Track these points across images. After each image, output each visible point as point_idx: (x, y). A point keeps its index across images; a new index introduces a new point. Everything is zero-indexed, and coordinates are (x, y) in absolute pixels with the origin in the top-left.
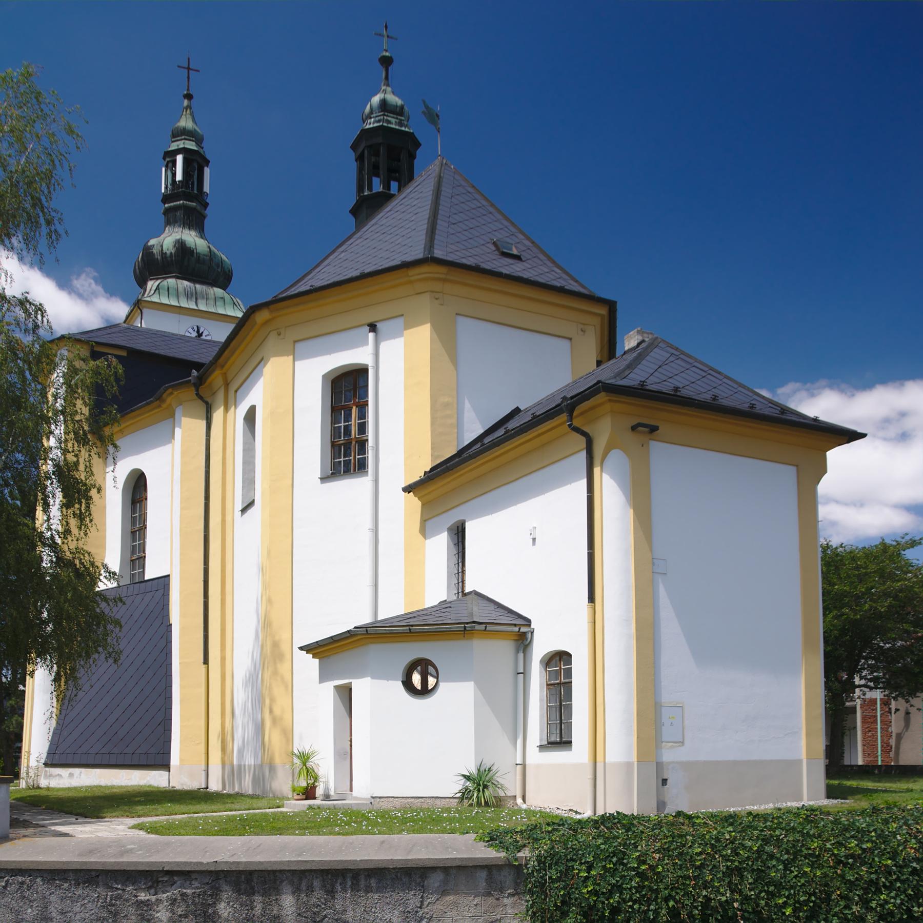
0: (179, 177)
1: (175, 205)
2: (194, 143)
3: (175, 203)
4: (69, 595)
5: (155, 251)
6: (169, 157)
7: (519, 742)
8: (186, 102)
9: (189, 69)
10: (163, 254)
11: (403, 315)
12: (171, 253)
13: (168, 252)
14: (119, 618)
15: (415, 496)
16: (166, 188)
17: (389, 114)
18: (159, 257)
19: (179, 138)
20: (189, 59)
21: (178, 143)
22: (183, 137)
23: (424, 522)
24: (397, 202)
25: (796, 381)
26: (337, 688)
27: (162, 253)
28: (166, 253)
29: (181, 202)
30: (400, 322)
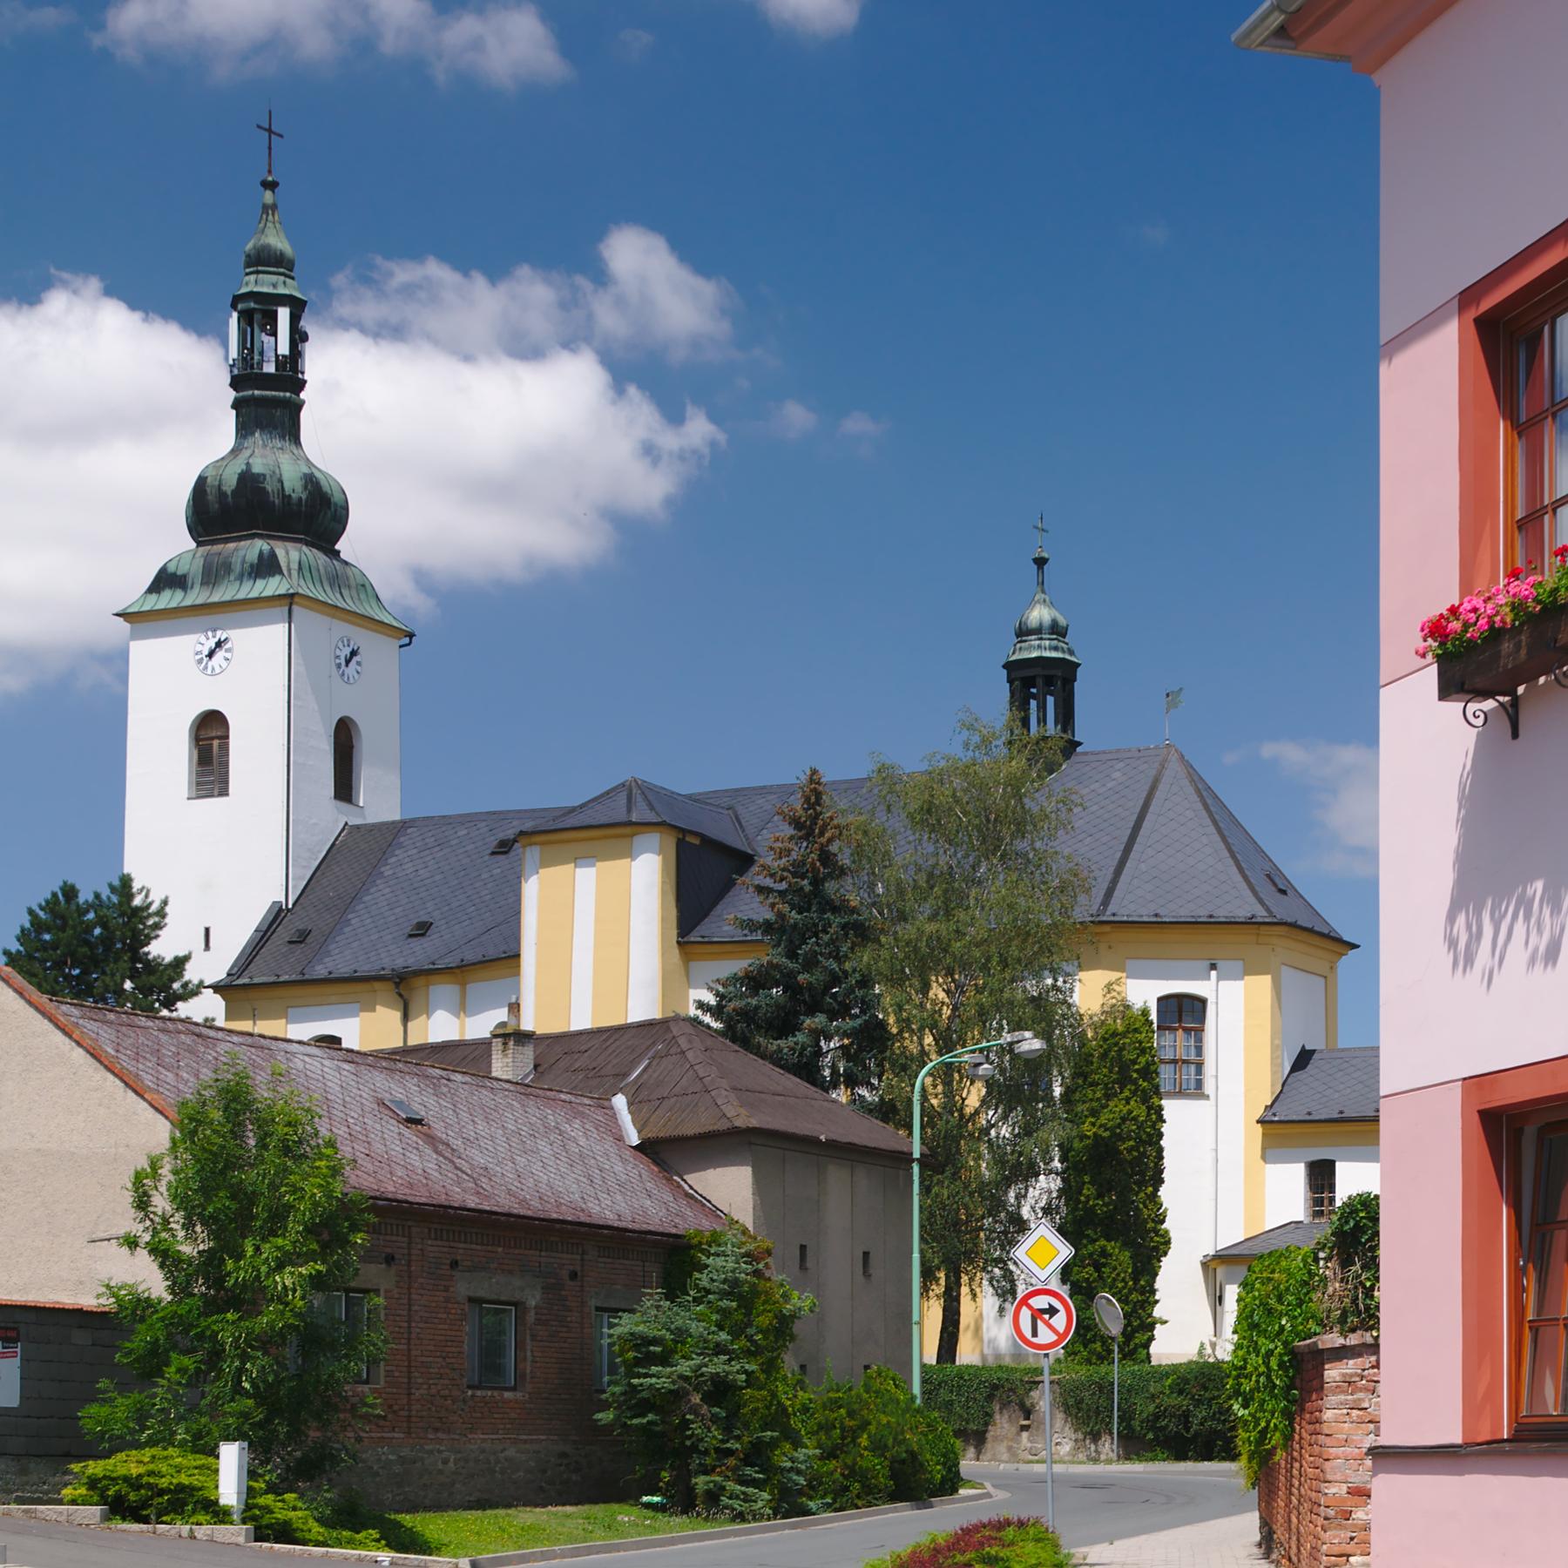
3: (273, 393)
4: (47, 937)
5: (269, 488)
6: (255, 303)
8: (268, 197)
10: (286, 498)
11: (1243, 960)
12: (300, 499)
13: (293, 495)
17: (1030, 638)
18: (277, 501)
20: (270, 112)
21: (274, 278)
22: (282, 270)
23: (1264, 1149)
24: (1272, 28)
28: (290, 496)
29: (288, 394)
30: (357, 1006)
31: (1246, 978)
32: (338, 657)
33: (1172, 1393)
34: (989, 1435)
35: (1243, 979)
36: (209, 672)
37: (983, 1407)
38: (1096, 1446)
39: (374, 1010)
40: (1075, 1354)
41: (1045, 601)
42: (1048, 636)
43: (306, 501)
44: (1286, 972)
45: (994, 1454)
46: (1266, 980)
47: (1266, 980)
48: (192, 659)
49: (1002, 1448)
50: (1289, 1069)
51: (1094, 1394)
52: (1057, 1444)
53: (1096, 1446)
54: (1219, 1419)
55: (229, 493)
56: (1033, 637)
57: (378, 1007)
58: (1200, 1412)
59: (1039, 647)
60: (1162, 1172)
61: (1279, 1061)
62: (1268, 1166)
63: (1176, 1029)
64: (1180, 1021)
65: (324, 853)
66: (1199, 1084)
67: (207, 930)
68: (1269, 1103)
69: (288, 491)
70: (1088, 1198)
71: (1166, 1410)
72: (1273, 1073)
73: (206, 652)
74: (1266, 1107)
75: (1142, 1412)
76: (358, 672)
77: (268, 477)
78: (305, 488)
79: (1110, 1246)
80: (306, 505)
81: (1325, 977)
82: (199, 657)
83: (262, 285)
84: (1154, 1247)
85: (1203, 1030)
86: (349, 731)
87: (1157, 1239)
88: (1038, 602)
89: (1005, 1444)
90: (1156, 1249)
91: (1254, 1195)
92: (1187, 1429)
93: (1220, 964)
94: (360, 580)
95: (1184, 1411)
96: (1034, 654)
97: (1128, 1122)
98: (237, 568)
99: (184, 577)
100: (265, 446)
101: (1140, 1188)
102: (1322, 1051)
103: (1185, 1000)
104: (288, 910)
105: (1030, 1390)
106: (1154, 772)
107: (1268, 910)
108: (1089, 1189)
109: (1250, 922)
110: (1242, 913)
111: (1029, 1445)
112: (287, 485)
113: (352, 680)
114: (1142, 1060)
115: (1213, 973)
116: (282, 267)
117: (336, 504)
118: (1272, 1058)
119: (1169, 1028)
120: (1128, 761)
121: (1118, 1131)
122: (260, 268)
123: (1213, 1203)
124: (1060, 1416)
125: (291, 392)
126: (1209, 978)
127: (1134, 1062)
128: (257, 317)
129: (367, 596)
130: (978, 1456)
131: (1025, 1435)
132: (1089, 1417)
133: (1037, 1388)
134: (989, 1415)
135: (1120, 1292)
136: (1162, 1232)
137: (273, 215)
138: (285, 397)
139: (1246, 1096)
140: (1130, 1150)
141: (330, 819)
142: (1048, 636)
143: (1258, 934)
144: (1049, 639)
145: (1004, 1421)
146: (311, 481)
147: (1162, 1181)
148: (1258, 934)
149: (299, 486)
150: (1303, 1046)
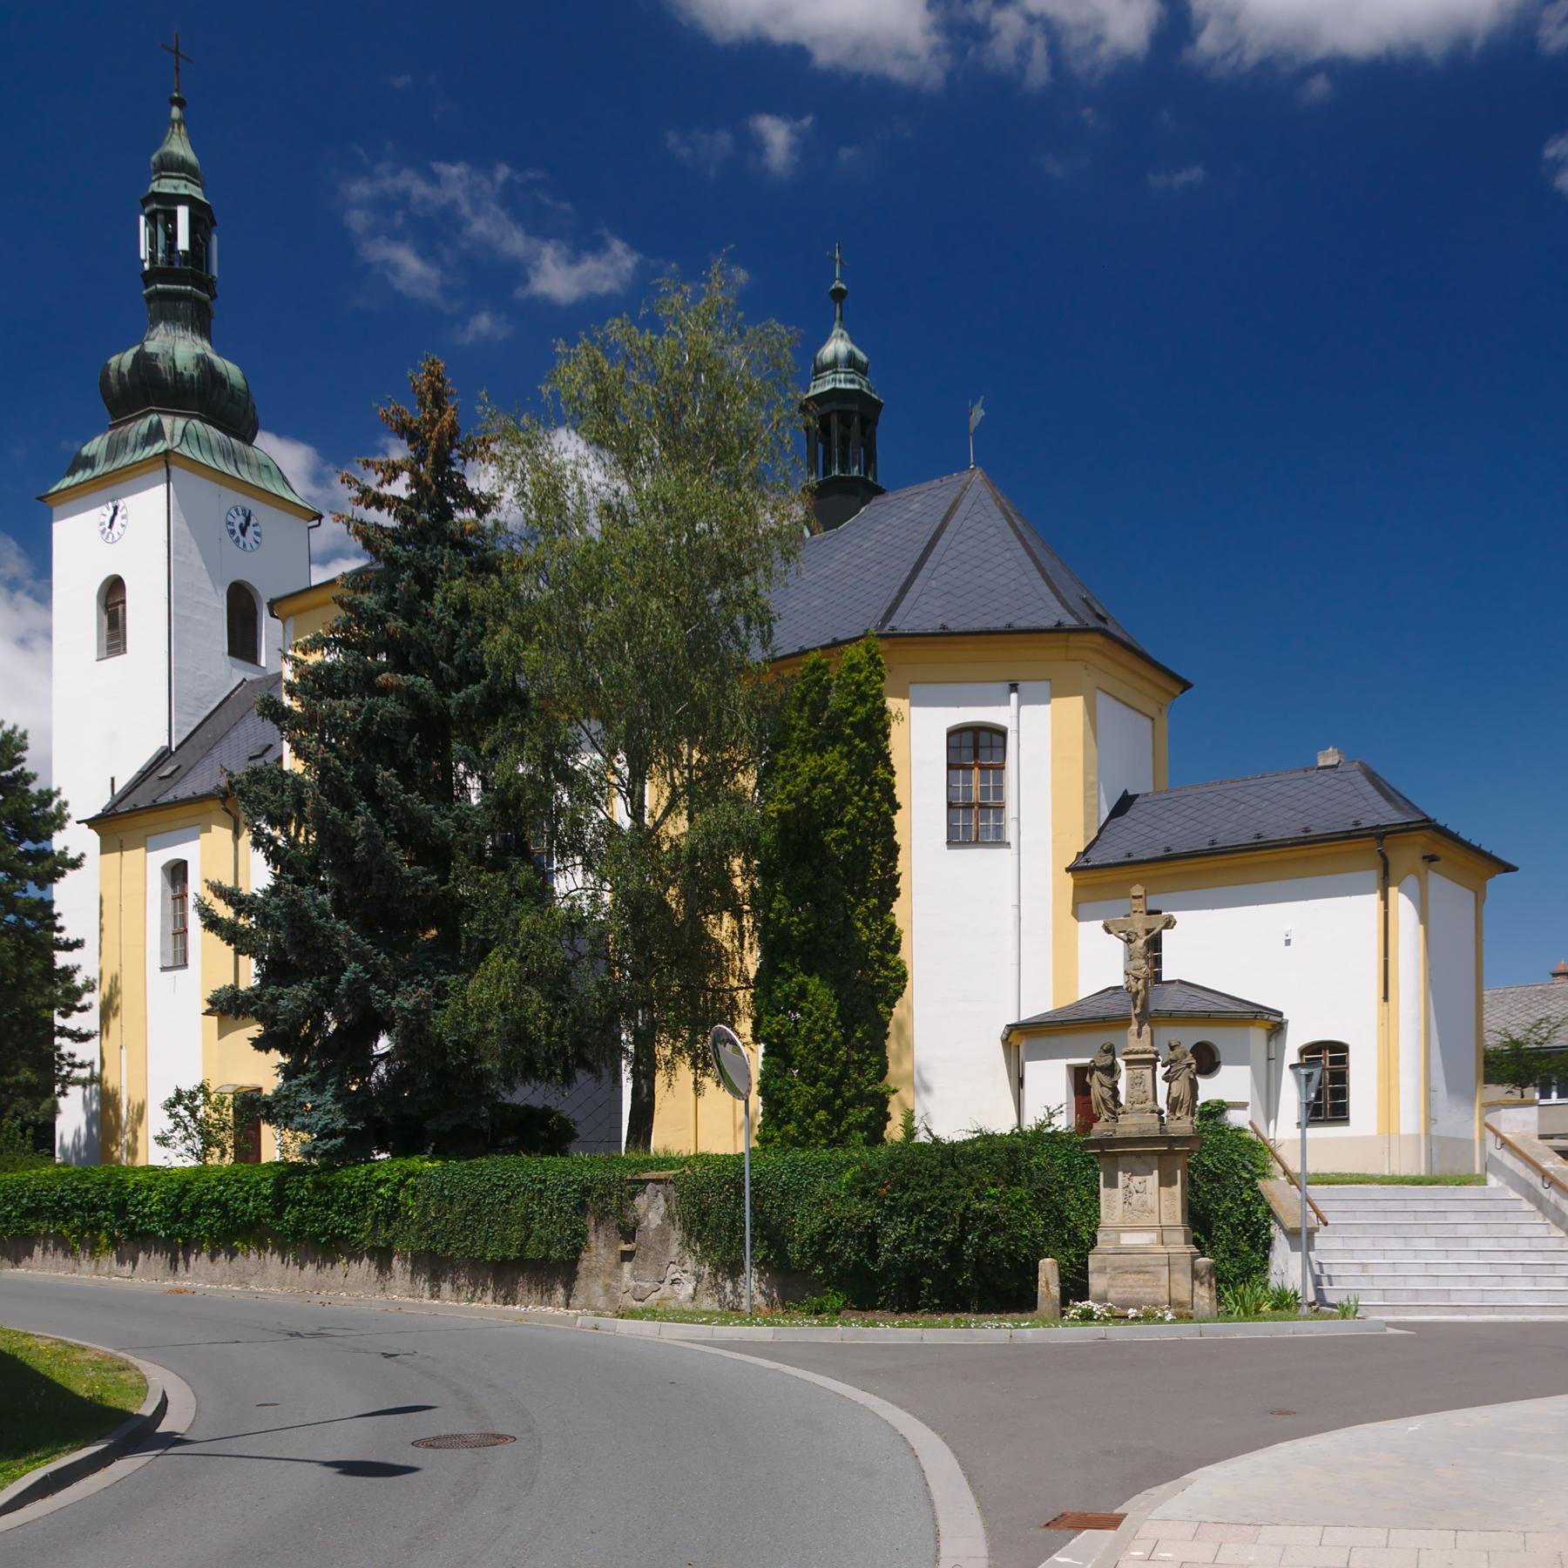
0: (183, 243)
1: (175, 290)
2: (199, 190)
3: (175, 287)
5: (161, 366)
6: (158, 203)
7: (1272, 1122)
9: (177, 52)
10: (177, 375)
11: (1050, 680)
12: (192, 376)
14: (1525, 1090)
15: (1073, 876)
16: (153, 257)
17: (824, 374)
18: (169, 378)
19: (174, 174)
21: (176, 182)
22: (183, 175)
23: (1076, 904)
25: (97, 435)
26: (1068, 1066)
27: (176, 373)
28: (182, 373)
29: (189, 288)
31: (1053, 700)
32: (232, 524)
33: (852, 1195)
34: (581, 1267)
35: (1049, 703)
36: (110, 540)
37: (569, 1221)
38: (735, 1283)
39: (210, 831)
40: (771, 1140)
41: (842, 335)
42: (843, 370)
43: (198, 377)
44: (1103, 700)
45: (587, 1297)
46: (1078, 702)
47: (1078, 702)
48: (98, 529)
49: (597, 1288)
50: (1107, 814)
51: (728, 1198)
52: (673, 1282)
53: (735, 1283)
54: (926, 1241)
55: (126, 373)
56: (828, 373)
57: (214, 827)
58: (894, 1230)
59: (834, 380)
60: (896, 879)
61: (1094, 801)
62: (1081, 923)
63: (971, 768)
64: (976, 756)
65: (216, 704)
66: (999, 830)
67: (113, 779)
68: (1082, 850)
69: (180, 367)
70: (779, 914)
71: (838, 1224)
72: (1087, 815)
73: (108, 524)
74: (1079, 854)
75: (801, 1231)
76: (257, 542)
77: (160, 357)
78: (197, 366)
79: (813, 984)
80: (199, 383)
81: (1153, 719)
82: (102, 528)
83: (164, 188)
84: (879, 985)
85: (1004, 768)
86: (248, 592)
87: (884, 973)
88: (836, 336)
89: (601, 1282)
90: (883, 987)
91: (1065, 959)
92: (874, 1256)
93: (1021, 686)
94: (263, 460)
95: (867, 1227)
96: (829, 387)
97: (820, 785)
98: (132, 441)
99: (94, 457)
100: (167, 334)
101: (858, 899)
102: (1146, 795)
103: (982, 734)
104: (172, 753)
105: (633, 1196)
106: (954, 496)
107: (1078, 619)
108: (780, 901)
109: (1059, 629)
110: (1048, 623)
111: (633, 1283)
112: (179, 364)
113: (248, 547)
114: (861, 711)
115: (1014, 696)
116: (183, 172)
117: (232, 386)
118: (1085, 797)
119: (963, 767)
120: (927, 493)
121: (806, 800)
122: (163, 173)
123: (1016, 968)
124: (676, 1235)
125: (193, 286)
126: (1008, 703)
127: (849, 712)
128: (160, 217)
129: (271, 476)
130: (568, 1300)
131: (627, 1266)
132: (718, 1238)
133: (644, 1191)
134: (584, 1236)
135: (819, 1047)
136: (893, 963)
137: (179, 128)
138: (186, 290)
139: (1053, 842)
140: (840, 841)
141: (228, 675)
142: (843, 370)
143: (1067, 647)
144: (845, 373)
145: (601, 1245)
146: (204, 360)
147: (896, 894)
148: (1067, 647)
149: (191, 365)
150: (1126, 791)
